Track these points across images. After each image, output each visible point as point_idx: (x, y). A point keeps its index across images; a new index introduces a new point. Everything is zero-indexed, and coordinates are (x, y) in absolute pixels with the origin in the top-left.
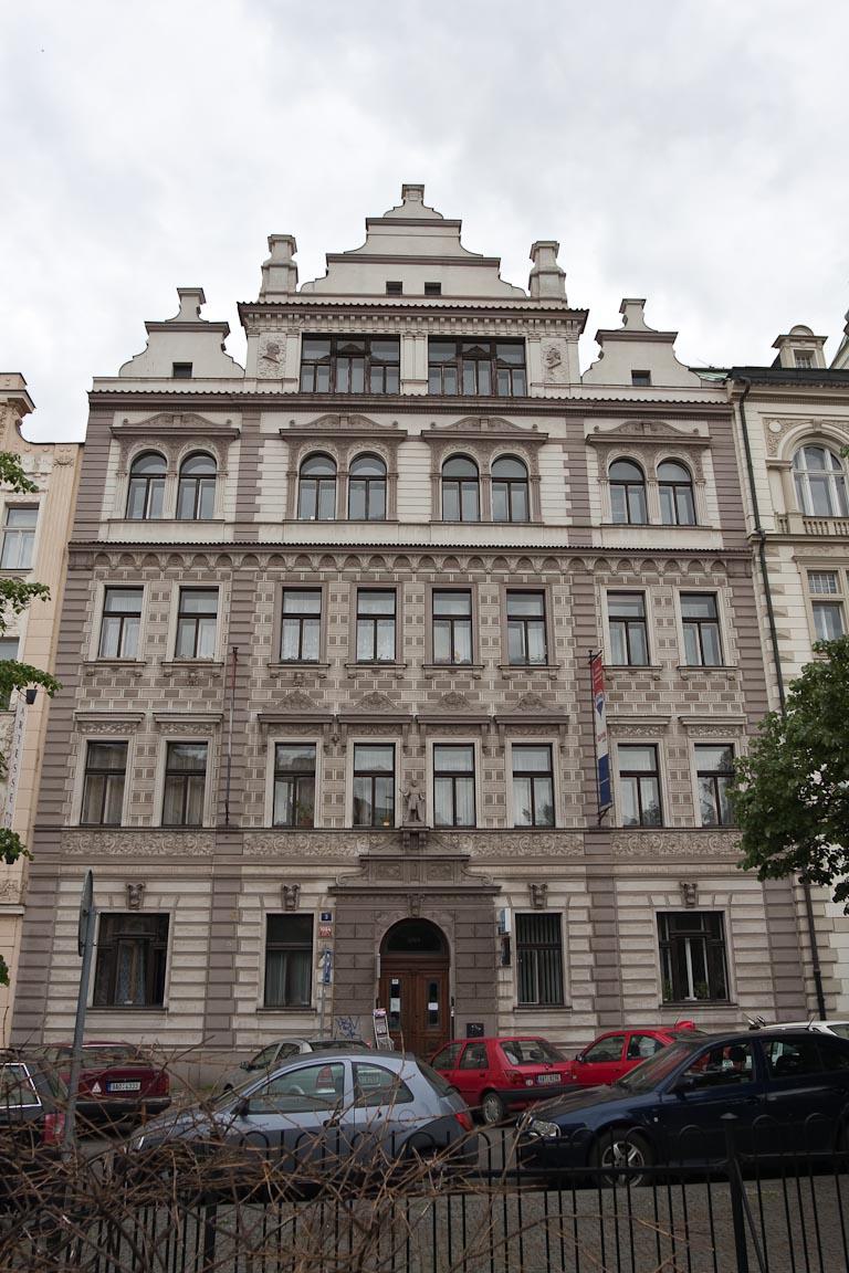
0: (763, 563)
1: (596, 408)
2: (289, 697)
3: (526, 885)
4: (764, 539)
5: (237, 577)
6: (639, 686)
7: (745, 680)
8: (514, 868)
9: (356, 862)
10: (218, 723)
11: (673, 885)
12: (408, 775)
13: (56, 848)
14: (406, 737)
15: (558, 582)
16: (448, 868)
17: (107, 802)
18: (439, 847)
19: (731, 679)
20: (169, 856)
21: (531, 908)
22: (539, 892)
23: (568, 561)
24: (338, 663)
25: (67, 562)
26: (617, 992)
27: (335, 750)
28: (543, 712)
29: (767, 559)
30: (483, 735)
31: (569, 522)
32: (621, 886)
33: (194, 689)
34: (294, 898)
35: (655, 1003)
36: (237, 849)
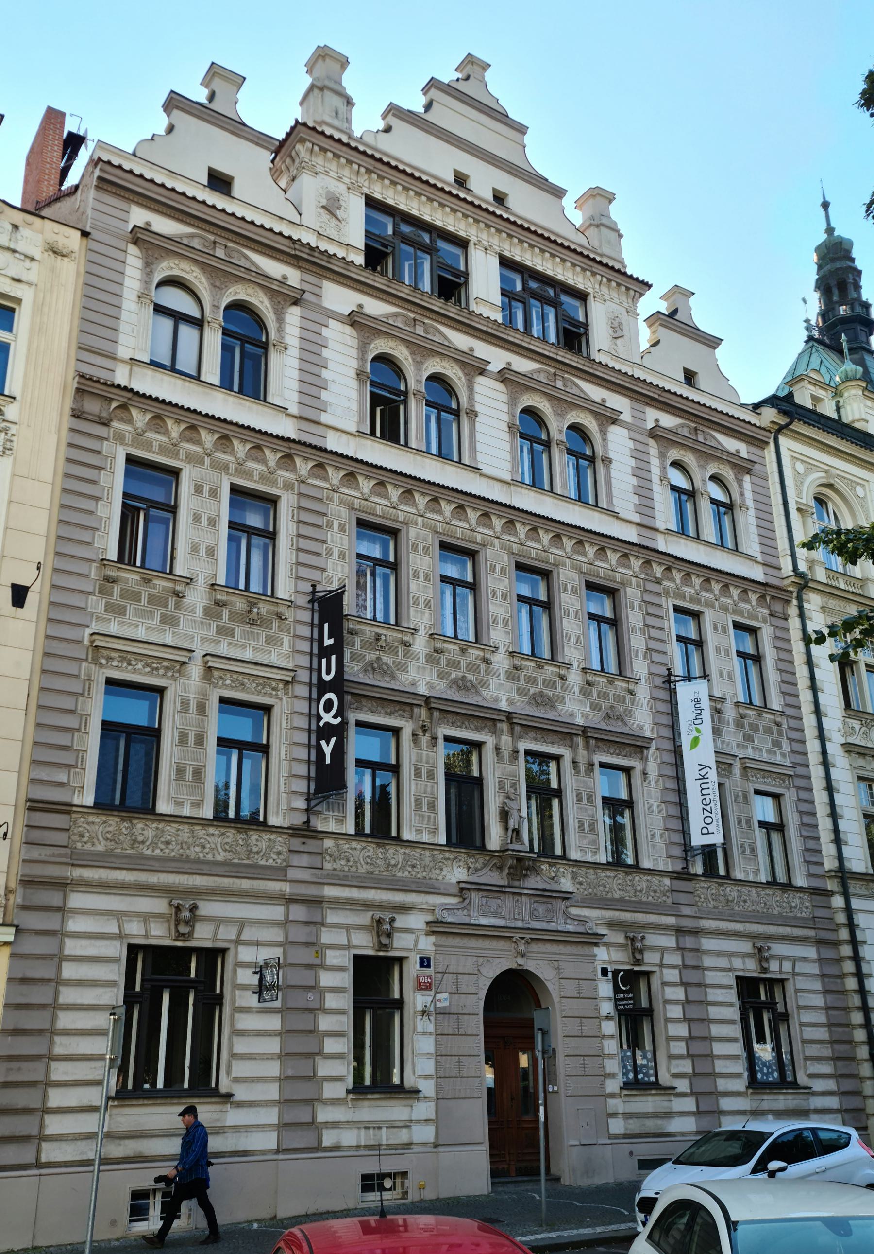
0: (801, 607)
1: (661, 399)
2: (370, 664)
3: (623, 936)
4: (807, 583)
5: (304, 489)
6: (152, 600)
7: (789, 728)
8: (748, 925)
9: (455, 891)
10: (287, 683)
11: (159, 905)
12: (502, 785)
13: (60, 838)
14: (498, 738)
15: (493, 545)
16: (550, 906)
17: (120, 767)
18: (539, 878)
19: (778, 725)
20: (225, 863)
21: (628, 963)
22: (638, 945)
23: (619, 554)
24: (422, 631)
25: (69, 404)
26: (840, 1064)
27: (425, 740)
28: (551, 715)
29: (805, 605)
30: (573, 747)
31: (636, 518)
32: (77, 900)
33: (255, 629)
34: (389, 935)
35: (94, 1096)
36: (316, 861)
